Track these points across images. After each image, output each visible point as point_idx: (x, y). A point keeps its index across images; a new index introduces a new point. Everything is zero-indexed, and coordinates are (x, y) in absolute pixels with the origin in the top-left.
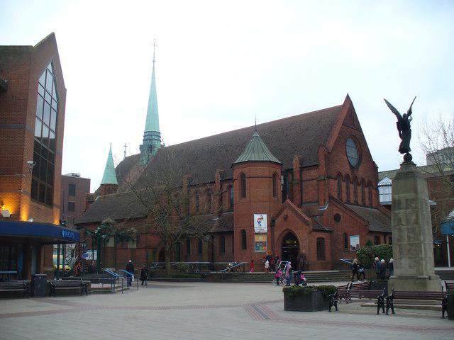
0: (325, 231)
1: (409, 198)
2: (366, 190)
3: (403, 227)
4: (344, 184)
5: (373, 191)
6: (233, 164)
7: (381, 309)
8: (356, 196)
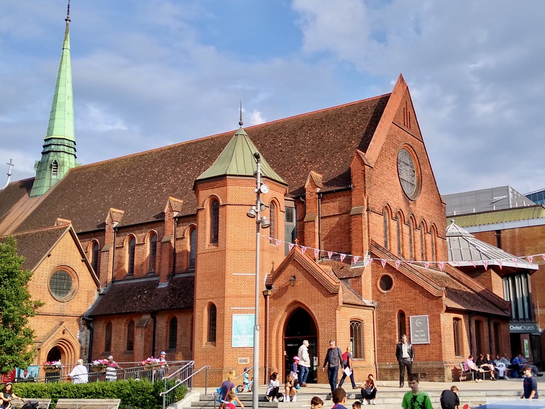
2: (428, 237)
4: (394, 224)
5: (439, 241)
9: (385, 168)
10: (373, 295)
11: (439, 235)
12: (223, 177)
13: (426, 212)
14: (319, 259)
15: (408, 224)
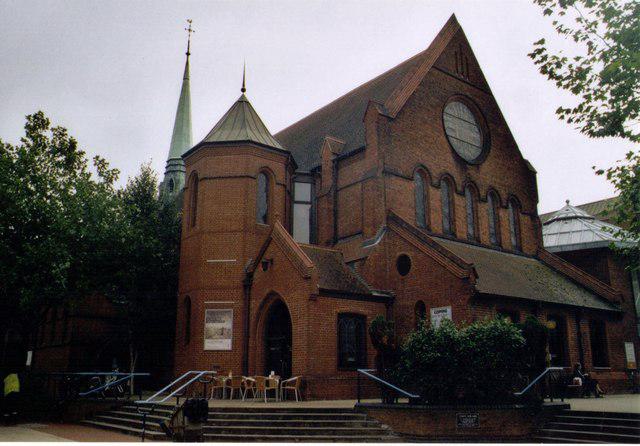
0: (369, 298)
5: (525, 219)
8: (476, 223)
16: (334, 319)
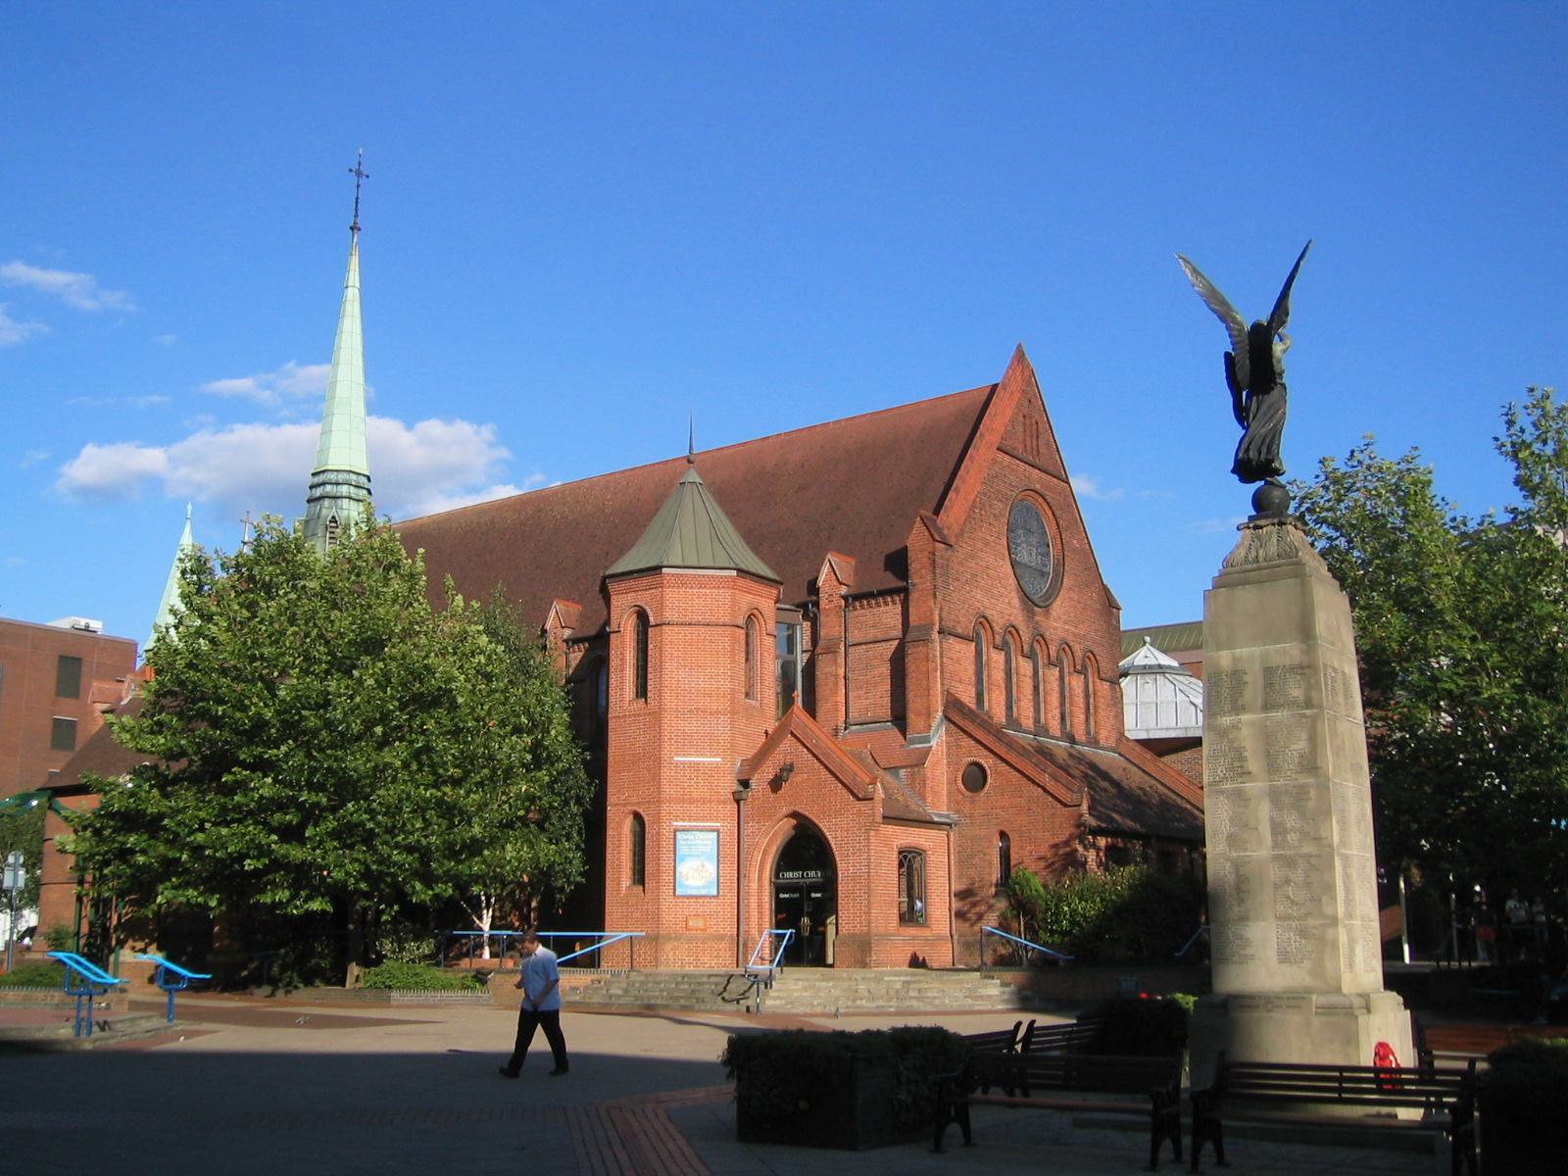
1: (1276, 660)
3: (1255, 787)
6: (604, 579)
7: (1167, 1144)
9: (979, 545)
10: (949, 801)
11: (1103, 676)
12: (656, 569)
13: (1073, 629)
14: (846, 729)
15: (1031, 656)
16: (895, 855)
